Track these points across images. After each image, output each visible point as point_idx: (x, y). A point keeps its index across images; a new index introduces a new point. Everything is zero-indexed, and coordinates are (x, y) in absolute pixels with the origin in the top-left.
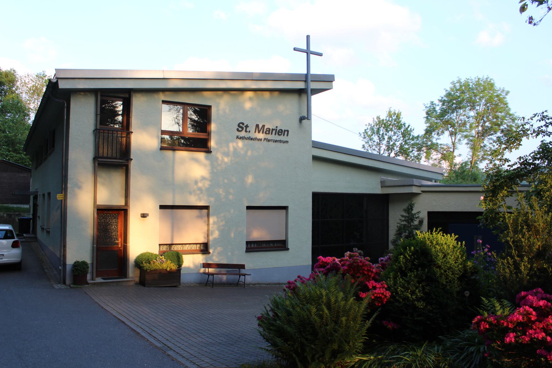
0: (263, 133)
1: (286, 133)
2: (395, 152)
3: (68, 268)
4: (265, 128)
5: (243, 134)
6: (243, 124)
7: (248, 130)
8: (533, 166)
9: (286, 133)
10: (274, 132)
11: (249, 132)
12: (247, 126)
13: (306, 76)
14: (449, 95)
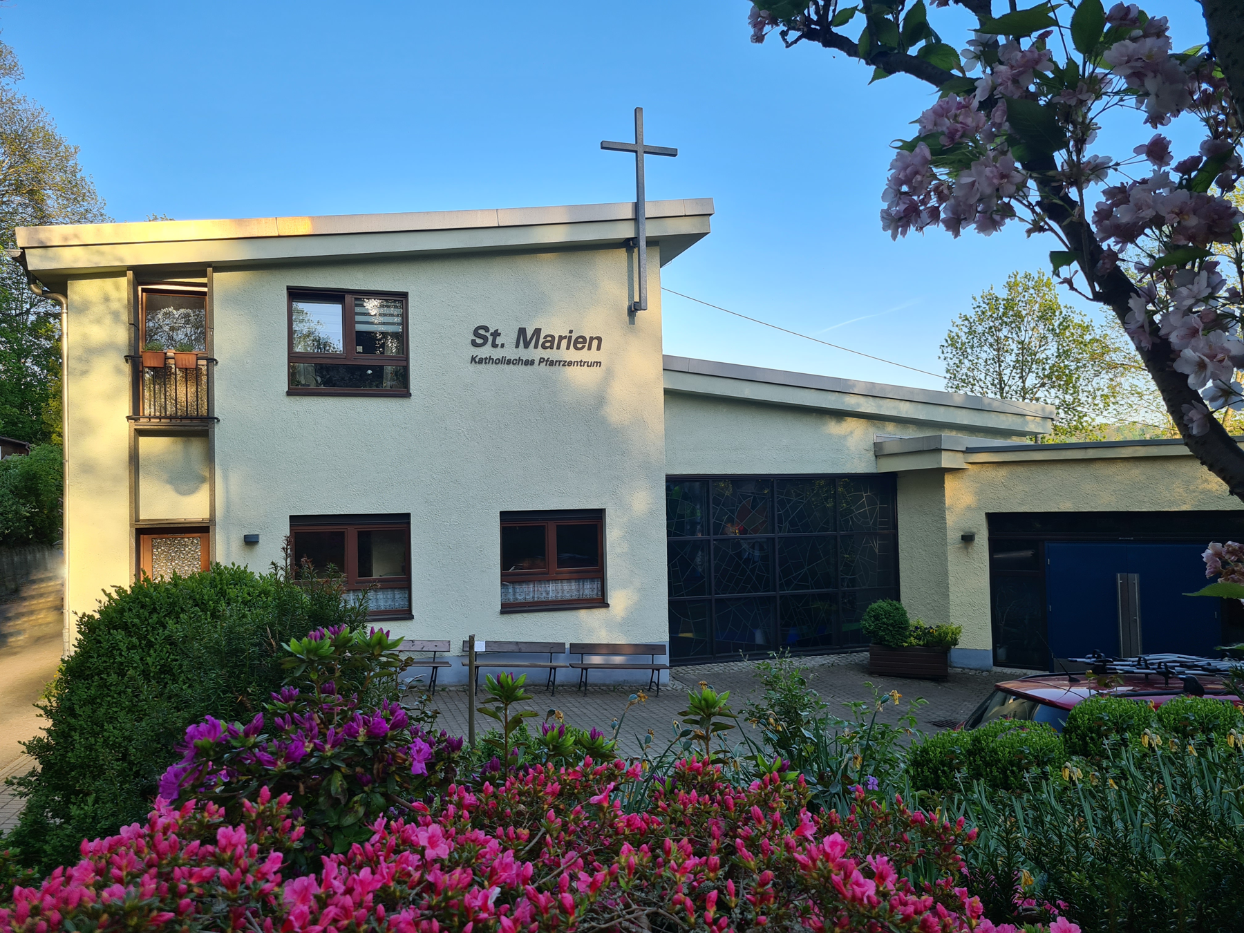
1: (595, 343)
4: (542, 336)
5: (486, 351)
6: (486, 328)
9: (595, 343)
10: (564, 343)
11: (503, 345)
12: (496, 334)
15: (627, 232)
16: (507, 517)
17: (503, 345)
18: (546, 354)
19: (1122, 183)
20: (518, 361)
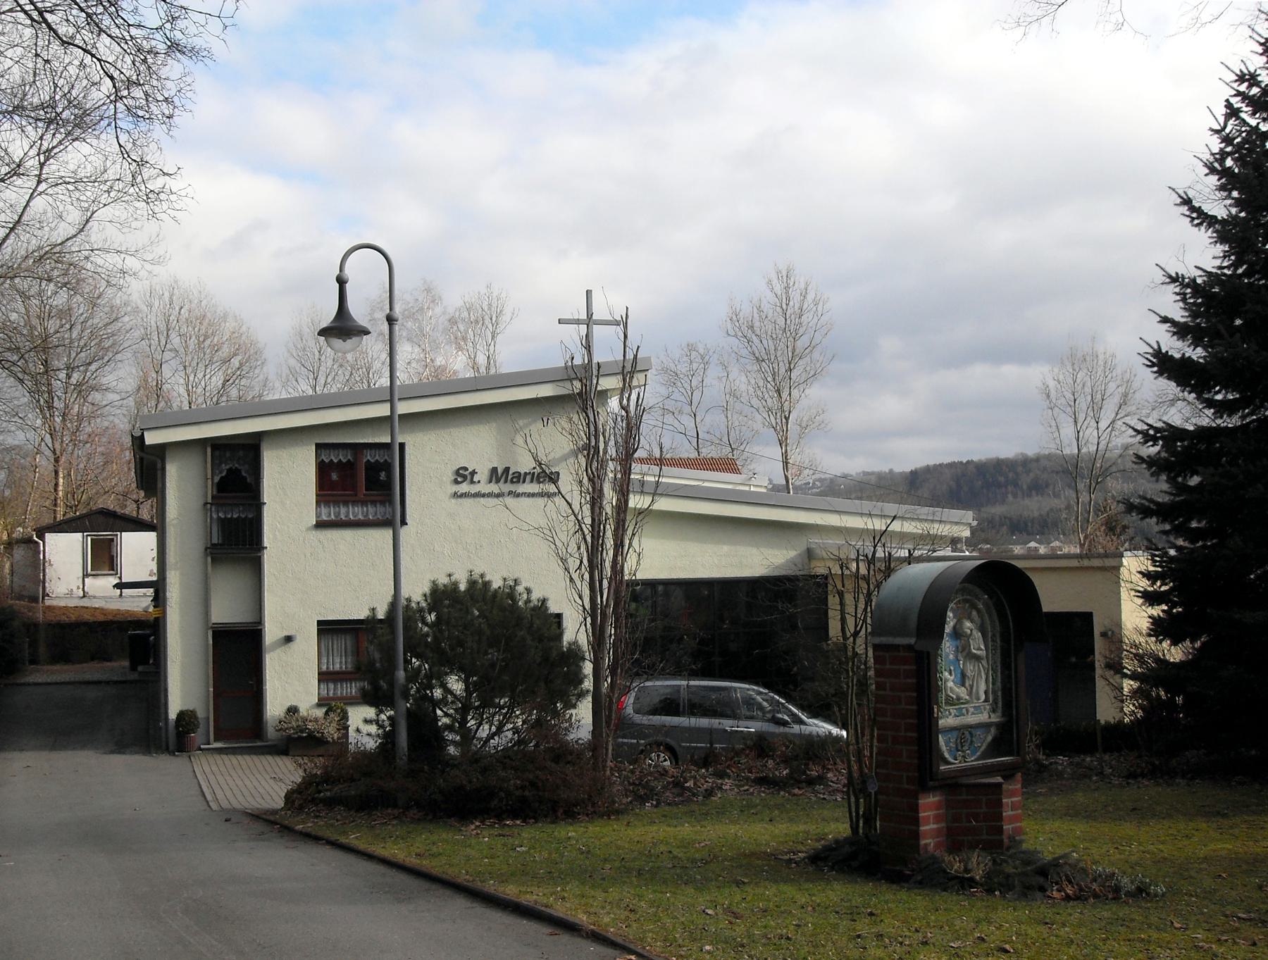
0: (506, 482)
2: (964, 654)
3: (172, 724)
4: (511, 472)
5: (464, 488)
6: (466, 469)
7: (475, 479)
8: (497, 701)
10: (528, 478)
11: (479, 482)
12: (473, 473)
13: (587, 367)
14: (916, 470)
15: (383, 410)
16: (1092, 613)
17: (479, 482)
18: (512, 487)
19: (1177, 274)
20: (490, 495)
